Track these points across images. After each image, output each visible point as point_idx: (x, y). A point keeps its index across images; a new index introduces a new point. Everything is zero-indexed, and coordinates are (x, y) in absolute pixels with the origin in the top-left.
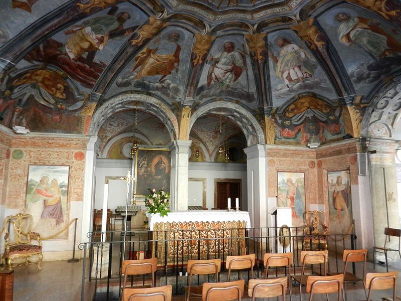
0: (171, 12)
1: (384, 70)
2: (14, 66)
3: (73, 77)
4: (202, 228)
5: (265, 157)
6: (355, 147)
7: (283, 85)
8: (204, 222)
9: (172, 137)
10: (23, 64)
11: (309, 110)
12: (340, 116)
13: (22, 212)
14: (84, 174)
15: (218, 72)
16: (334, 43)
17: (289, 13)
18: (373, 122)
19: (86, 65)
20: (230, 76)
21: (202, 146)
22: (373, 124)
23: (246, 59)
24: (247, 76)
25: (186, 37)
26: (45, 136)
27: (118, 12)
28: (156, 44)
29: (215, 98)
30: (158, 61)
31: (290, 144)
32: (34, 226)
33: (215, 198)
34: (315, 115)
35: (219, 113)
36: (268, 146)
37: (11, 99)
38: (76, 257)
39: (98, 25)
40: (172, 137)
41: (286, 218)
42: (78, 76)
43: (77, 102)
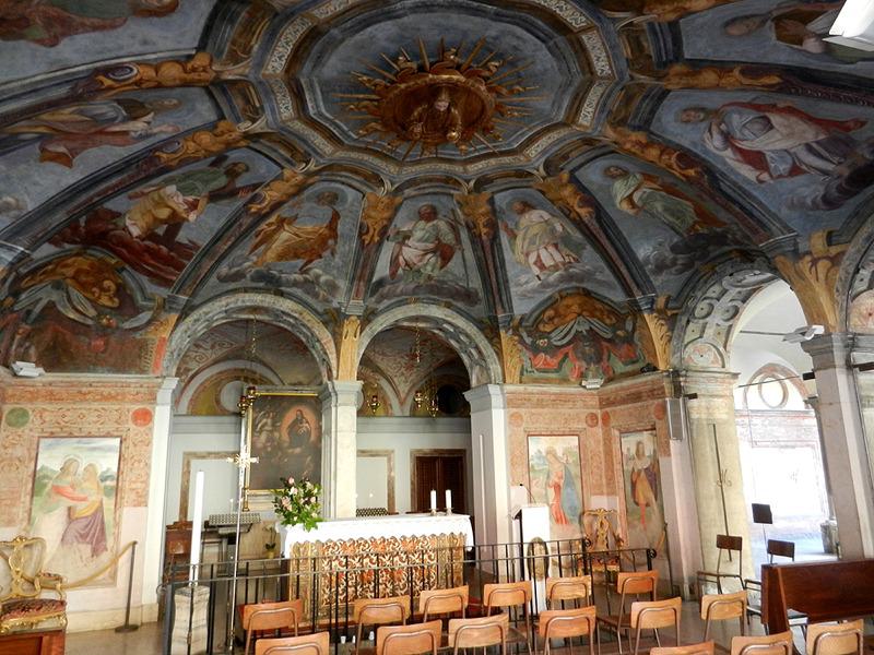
0: (322, 161)
1: (698, 254)
2: (29, 255)
3: (136, 267)
4: (384, 548)
5: (504, 408)
6: (663, 387)
7: (530, 275)
8: (386, 537)
9: (325, 373)
10: (47, 250)
12: (634, 330)
13: (23, 534)
14: (151, 452)
15: (410, 253)
18: (689, 343)
19: (161, 247)
21: (384, 383)
22: (690, 345)
23: (459, 233)
24: (464, 260)
25: (350, 199)
26: (73, 379)
30: (297, 235)
31: (548, 381)
32: (46, 562)
33: (413, 490)
35: (414, 325)
36: (508, 388)
37: (12, 312)
38: (131, 622)
40: (325, 373)
41: (539, 525)
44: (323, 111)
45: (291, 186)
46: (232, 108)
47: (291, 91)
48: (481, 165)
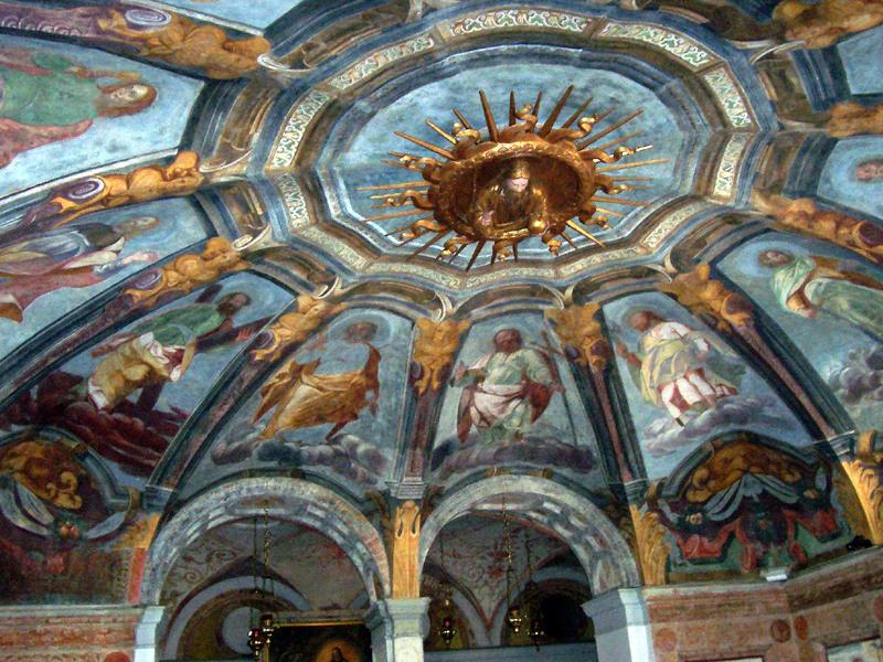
3: (103, 450)
7: (666, 420)
11: (750, 478)
15: (485, 402)
16: (771, 312)
17: (645, 260)
20: (520, 409)
26: (24, 614)
27: (222, 294)
28: (316, 350)
29: (485, 470)
30: (320, 389)
31: (708, 577)
34: (767, 488)
39: (170, 326)
42: (114, 448)
43: (109, 516)
44: (350, 210)
45: (310, 319)
46: (226, 221)
47: (305, 188)
48: (580, 265)
